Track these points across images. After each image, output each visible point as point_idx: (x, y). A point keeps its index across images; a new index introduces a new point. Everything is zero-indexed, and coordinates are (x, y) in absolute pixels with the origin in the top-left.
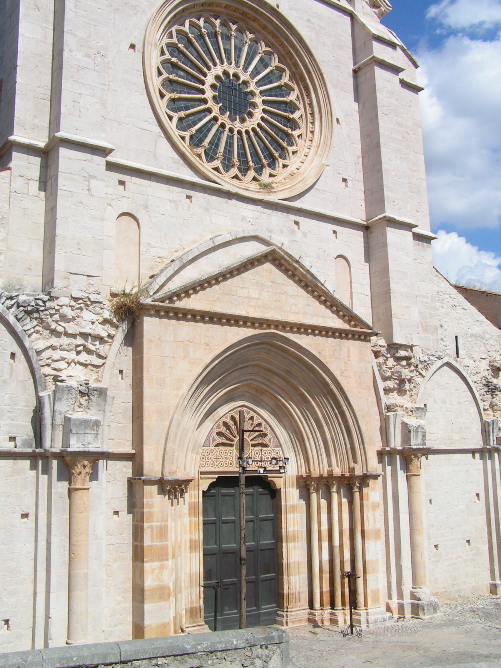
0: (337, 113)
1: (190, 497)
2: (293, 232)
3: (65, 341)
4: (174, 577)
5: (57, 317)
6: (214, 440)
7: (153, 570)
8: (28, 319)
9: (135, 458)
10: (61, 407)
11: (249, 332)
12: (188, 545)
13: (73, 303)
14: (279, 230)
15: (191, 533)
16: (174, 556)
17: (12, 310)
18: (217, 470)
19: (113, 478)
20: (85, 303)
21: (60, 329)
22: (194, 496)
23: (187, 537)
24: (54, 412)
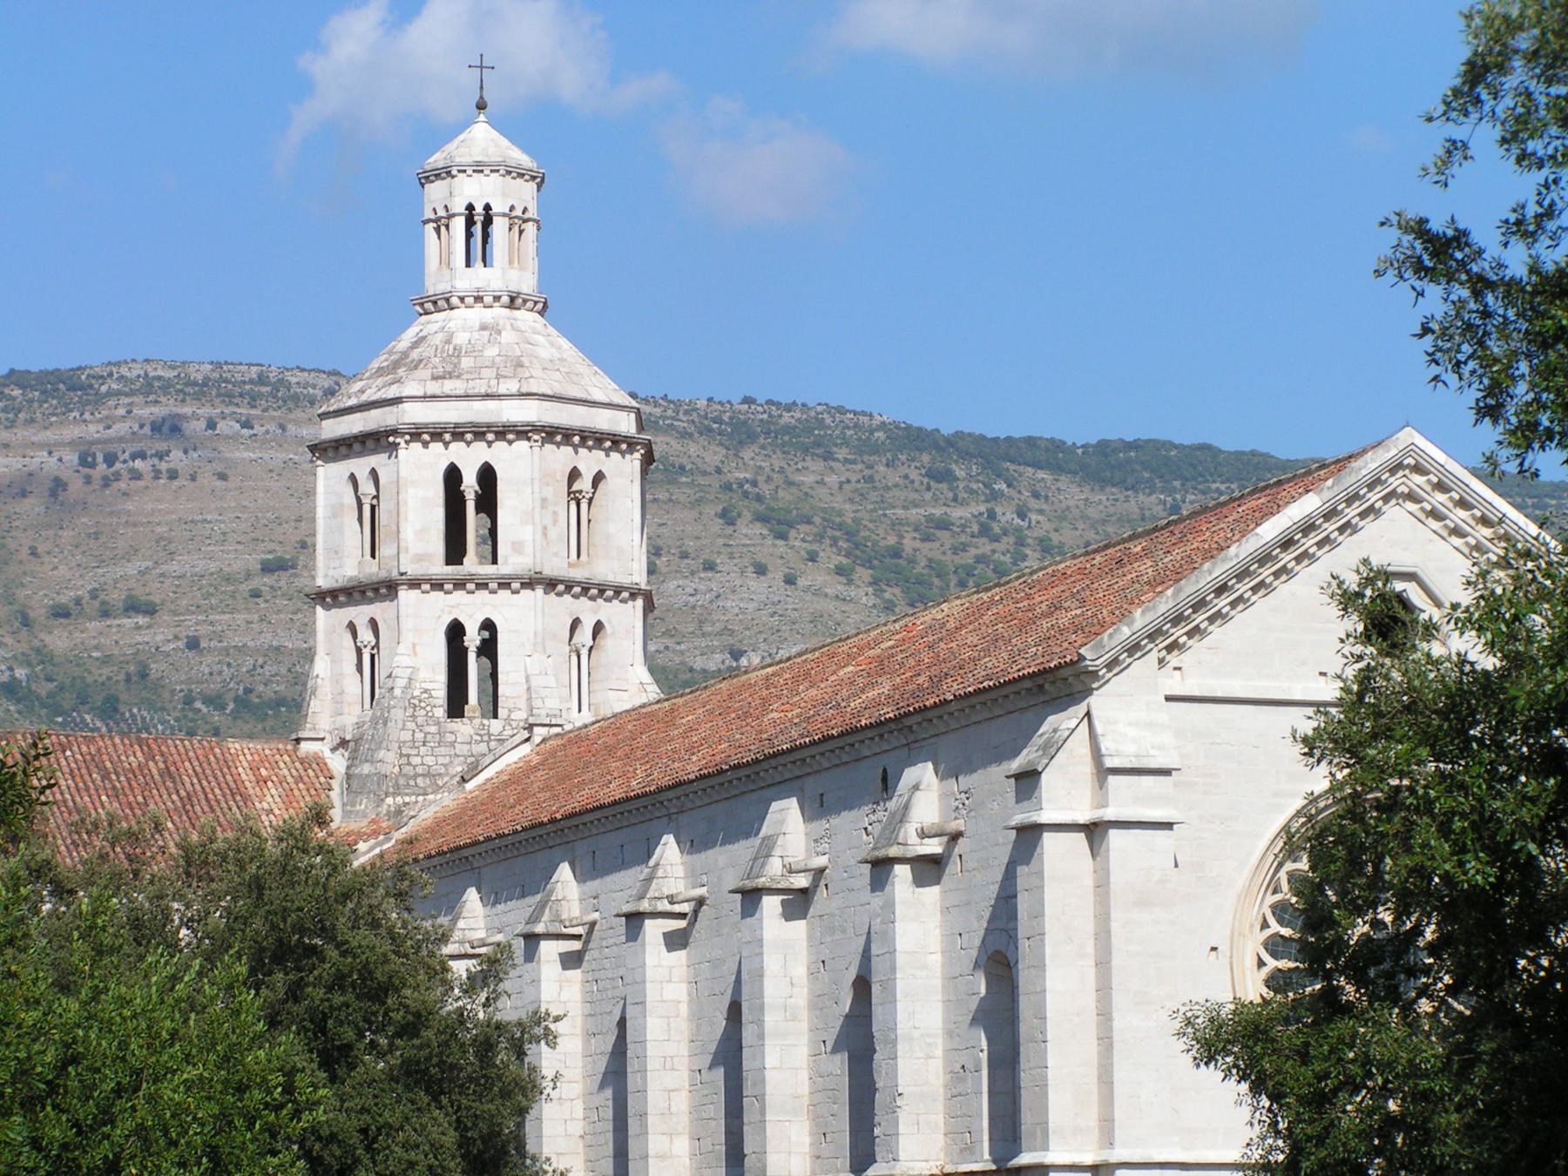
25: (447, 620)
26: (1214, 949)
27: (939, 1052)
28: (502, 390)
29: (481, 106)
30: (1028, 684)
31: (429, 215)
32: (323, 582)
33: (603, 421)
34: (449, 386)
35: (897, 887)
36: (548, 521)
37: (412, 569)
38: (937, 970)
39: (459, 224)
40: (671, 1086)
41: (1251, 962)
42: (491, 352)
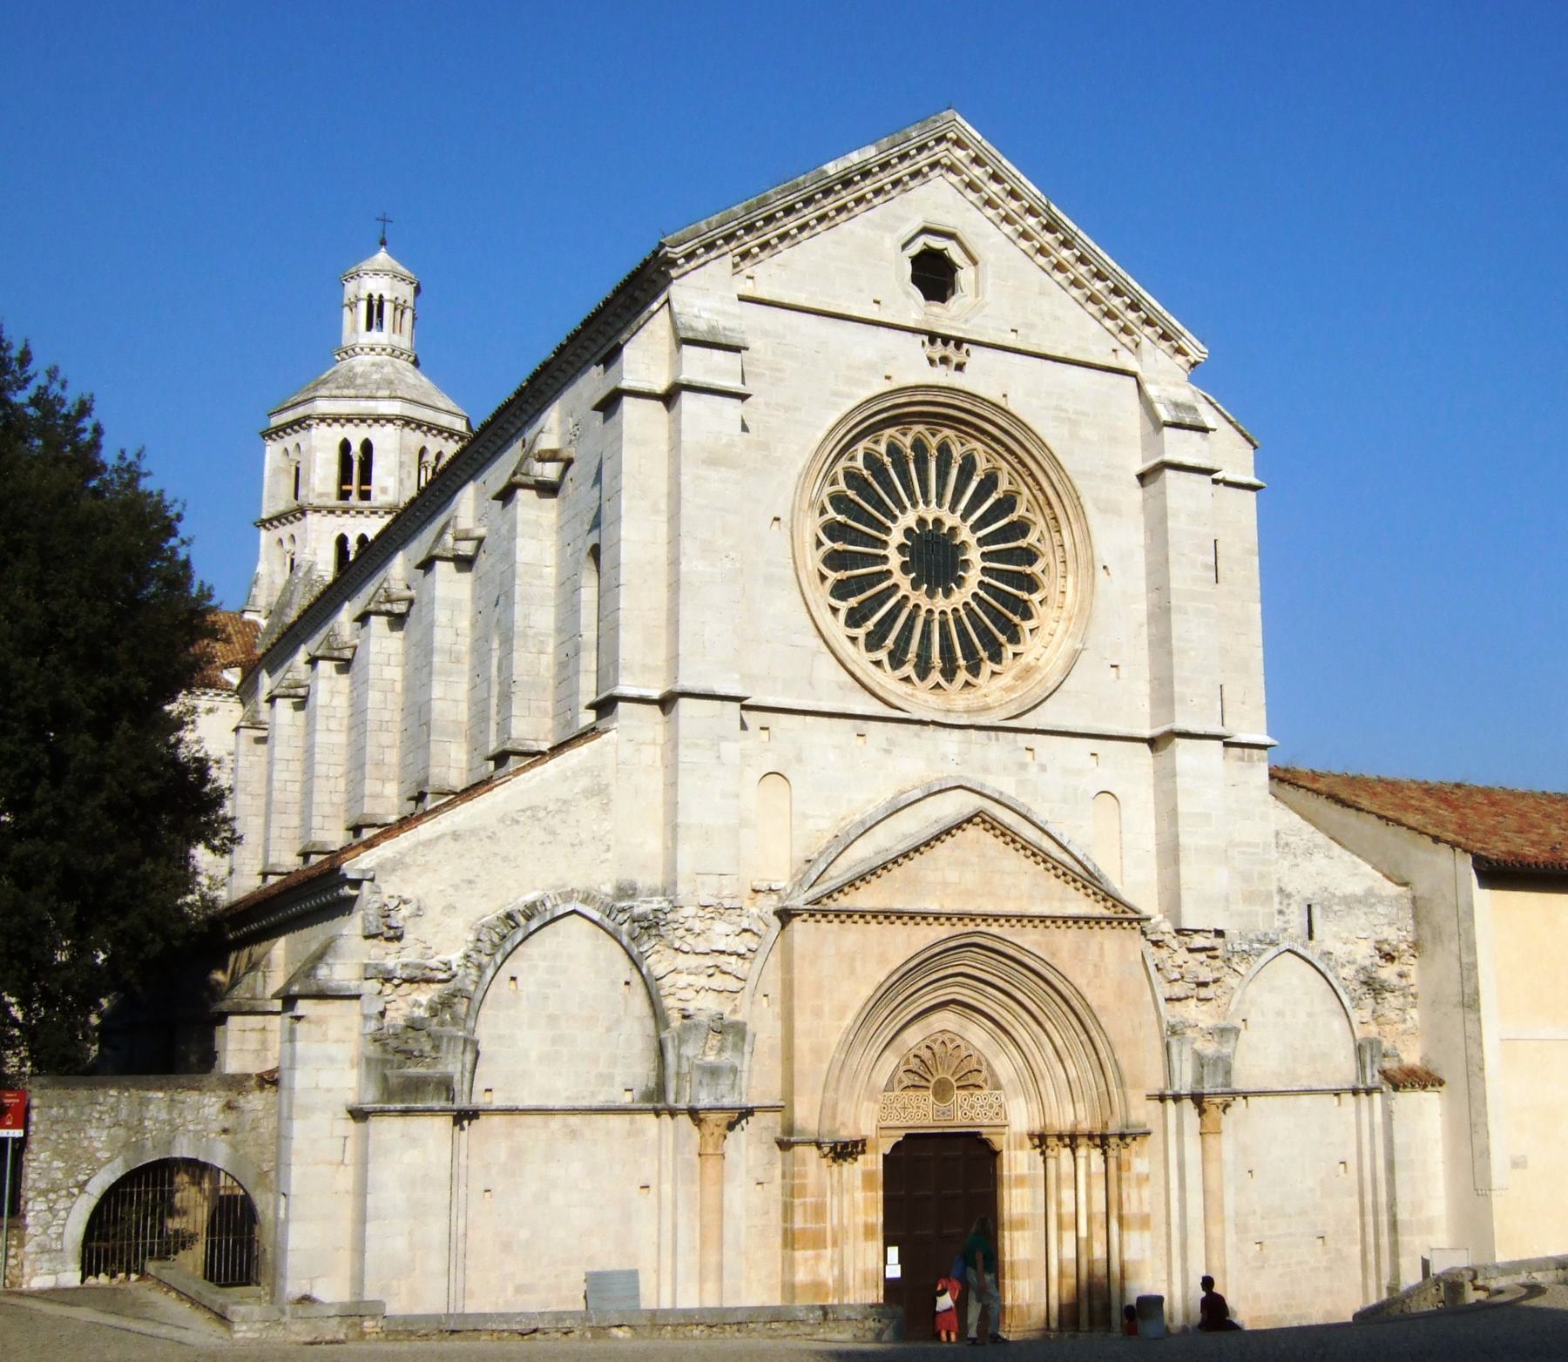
0: (1103, 553)
1: (866, 1163)
2: (1023, 766)
3: (693, 961)
4: (836, 1272)
5: (681, 932)
6: (900, 1082)
7: (806, 1260)
8: (645, 938)
9: (783, 1108)
10: (689, 1050)
11: (941, 931)
12: (861, 1230)
13: (701, 913)
14: (998, 767)
15: (866, 1214)
16: (834, 1244)
17: (626, 926)
18: (904, 1124)
19: (763, 1126)
20: (716, 910)
21: (685, 948)
22: (872, 1162)
23: (860, 1219)
24: (679, 1057)
25: (337, 534)
26: (777, 519)
27: (550, 648)
28: (379, 394)
29: (383, 243)
30: (622, 299)
31: (346, 301)
32: (265, 516)
33: (444, 420)
34: (346, 392)
35: (520, 509)
36: (404, 476)
37: (316, 502)
38: (552, 581)
39: (363, 306)
40: (385, 743)
41: (810, 541)
42: (376, 376)
